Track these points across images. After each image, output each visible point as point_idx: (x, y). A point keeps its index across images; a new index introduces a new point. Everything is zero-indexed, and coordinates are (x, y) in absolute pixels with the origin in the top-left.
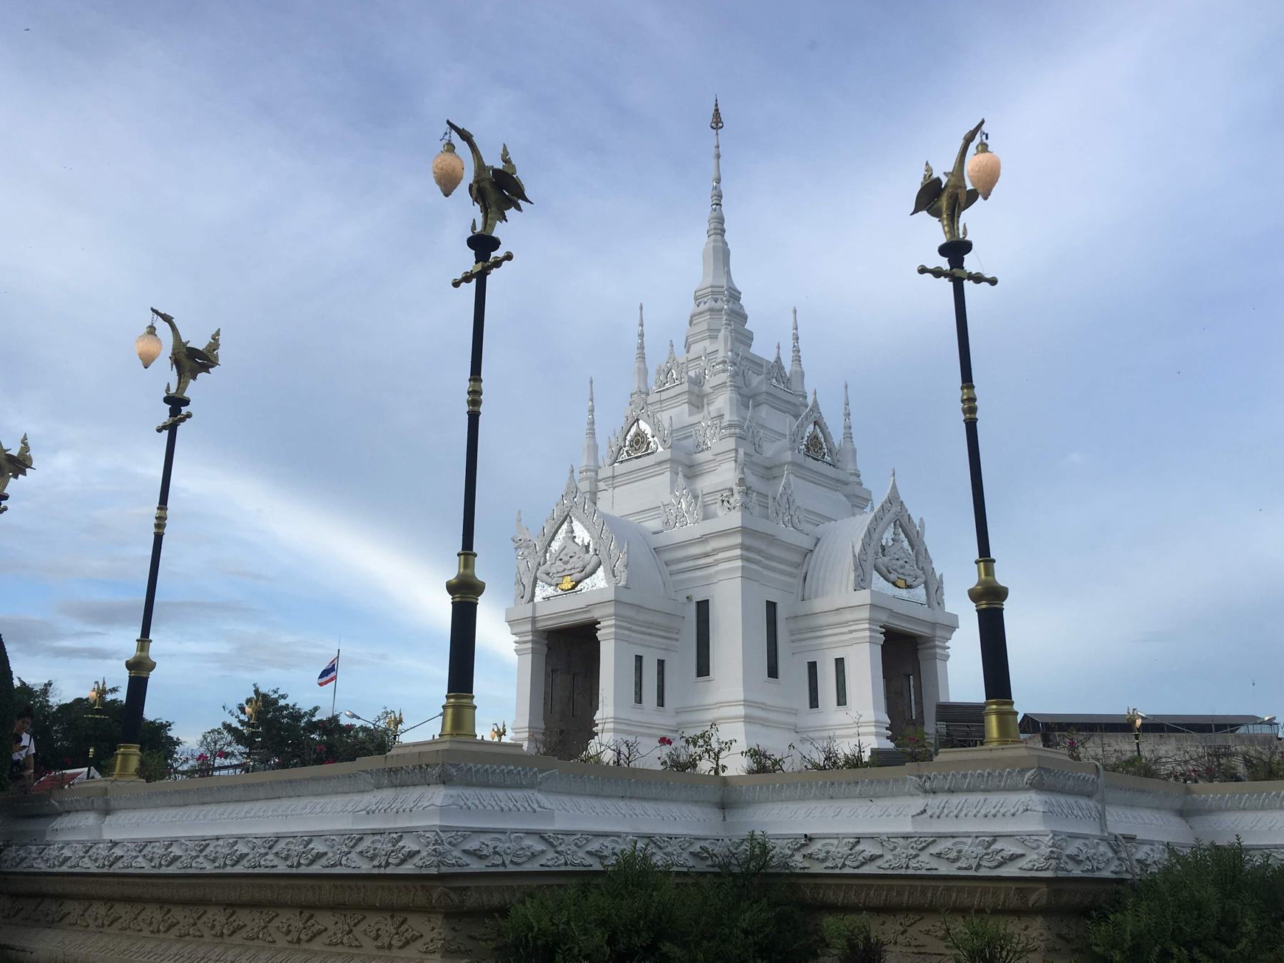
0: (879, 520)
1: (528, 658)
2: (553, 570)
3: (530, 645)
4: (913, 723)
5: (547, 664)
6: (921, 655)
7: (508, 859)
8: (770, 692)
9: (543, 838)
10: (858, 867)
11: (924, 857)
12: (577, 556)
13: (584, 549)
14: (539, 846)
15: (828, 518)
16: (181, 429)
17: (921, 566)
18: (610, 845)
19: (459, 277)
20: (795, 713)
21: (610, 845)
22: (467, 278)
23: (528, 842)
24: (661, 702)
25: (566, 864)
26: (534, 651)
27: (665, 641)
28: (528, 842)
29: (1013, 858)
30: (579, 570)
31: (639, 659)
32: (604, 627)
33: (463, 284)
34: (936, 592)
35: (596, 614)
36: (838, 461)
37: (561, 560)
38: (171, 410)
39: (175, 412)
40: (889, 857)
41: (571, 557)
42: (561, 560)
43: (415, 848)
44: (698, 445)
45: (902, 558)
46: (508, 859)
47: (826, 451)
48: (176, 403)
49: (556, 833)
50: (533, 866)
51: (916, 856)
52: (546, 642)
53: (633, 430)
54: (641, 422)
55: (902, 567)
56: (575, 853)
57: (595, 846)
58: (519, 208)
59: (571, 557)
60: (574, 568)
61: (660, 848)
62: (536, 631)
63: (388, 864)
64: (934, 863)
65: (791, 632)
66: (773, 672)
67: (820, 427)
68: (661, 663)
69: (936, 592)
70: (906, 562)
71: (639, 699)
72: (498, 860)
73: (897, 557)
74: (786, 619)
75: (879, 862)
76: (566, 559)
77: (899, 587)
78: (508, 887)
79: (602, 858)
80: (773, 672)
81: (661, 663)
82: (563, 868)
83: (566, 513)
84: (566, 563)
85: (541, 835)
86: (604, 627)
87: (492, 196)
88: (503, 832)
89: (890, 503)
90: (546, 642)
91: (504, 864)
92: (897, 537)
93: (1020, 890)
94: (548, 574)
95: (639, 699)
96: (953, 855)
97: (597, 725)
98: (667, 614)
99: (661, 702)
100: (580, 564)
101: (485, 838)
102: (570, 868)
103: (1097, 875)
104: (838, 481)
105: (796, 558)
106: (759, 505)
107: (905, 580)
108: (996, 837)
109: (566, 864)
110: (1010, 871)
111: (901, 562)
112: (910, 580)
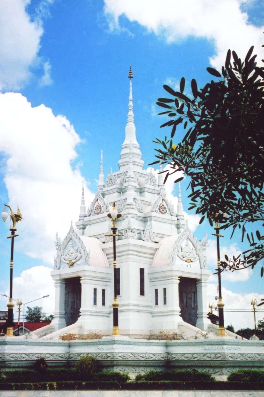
0: (183, 235)
1: (59, 289)
2: (66, 258)
5: (65, 290)
7: (18, 358)
8: (142, 300)
11: (205, 357)
13: (76, 251)
14: (152, 356)
15: (184, 225)
18: (233, 355)
19: (8, 237)
20: (151, 307)
21: (233, 355)
22: (10, 237)
23: (47, 355)
24: (104, 304)
26: (60, 287)
28: (47, 355)
29: (196, 357)
30: (74, 258)
31: (95, 290)
32: (83, 279)
33: (9, 238)
34: (204, 262)
35: (80, 275)
36: (172, 213)
37: (69, 254)
39: (13, 233)
40: (199, 357)
41: (72, 254)
42: (69, 254)
44: (119, 209)
46: (18, 358)
47: (167, 209)
48: (13, 231)
49: (29, 354)
51: (181, 357)
52: (65, 283)
53: (97, 204)
54: (99, 201)
55: (189, 255)
57: (37, 356)
59: (72, 254)
61: (52, 356)
62: (61, 279)
66: (142, 293)
67: (165, 201)
68: (104, 291)
69: (204, 262)
70: (191, 253)
71: (95, 303)
73: (187, 251)
74: (148, 274)
76: (70, 254)
77: (188, 262)
79: (38, 358)
80: (142, 293)
81: (104, 291)
84: (70, 256)
85: (25, 354)
86: (83, 279)
88: (18, 353)
89: (185, 232)
90: (65, 283)
91: (18, 359)
93: (111, 362)
94: (65, 259)
95: (95, 303)
96: (187, 357)
97: (81, 313)
99: (104, 304)
100: (75, 257)
101: (14, 355)
105: (153, 252)
106: (137, 233)
107: (190, 260)
108: (107, 353)
111: (189, 253)
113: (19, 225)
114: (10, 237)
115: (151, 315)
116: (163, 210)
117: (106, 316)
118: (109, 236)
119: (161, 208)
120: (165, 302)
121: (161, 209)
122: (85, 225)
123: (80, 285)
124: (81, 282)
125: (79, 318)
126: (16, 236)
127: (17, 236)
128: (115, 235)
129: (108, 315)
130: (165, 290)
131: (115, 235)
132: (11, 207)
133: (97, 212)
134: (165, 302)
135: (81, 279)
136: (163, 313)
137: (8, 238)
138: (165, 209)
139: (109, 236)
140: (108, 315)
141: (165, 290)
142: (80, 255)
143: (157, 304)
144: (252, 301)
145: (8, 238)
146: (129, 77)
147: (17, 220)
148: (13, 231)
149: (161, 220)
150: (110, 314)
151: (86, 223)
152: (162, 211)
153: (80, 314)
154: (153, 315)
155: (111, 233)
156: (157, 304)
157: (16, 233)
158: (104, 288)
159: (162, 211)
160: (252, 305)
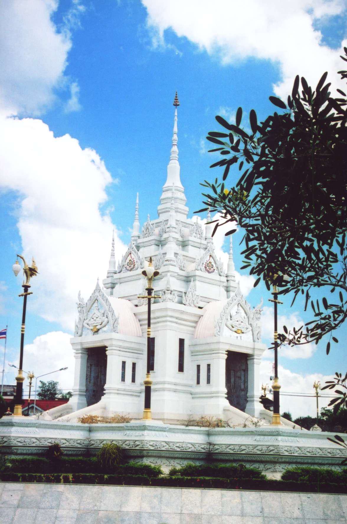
1: (79, 360)
2: (90, 323)
3: (80, 355)
4: (243, 390)
5: (88, 362)
6: (249, 362)
7: (27, 443)
9: (36, 439)
10: (241, 452)
12: (100, 317)
13: (102, 315)
16: (28, 296)
17: (250, 323)
22: (22, 295)
24: (133, 380)
25: (171, 449)
26: (82, 357)
27: (136, 355)
29: (244, 450)
31: (124, 363)
33: (21, 296)
37: (93, 318)
38: (25, 289)
41: (97, 318)
42: (93, 318)
43: (6, 440)
45: (240, 320)
46: (27, 443)
48: (26, 288)
50: (190, 450)
52: (87, 353)
53: (129, 258)
55: (240, 324)
56: (44, 442)
57: (50, 441)
58: (36, 275)
59: (97, 318)
60: (98, 323)
61: (68, 442)
63: (132, 447)
64: (257, 451)
65: (192, 353)
66: (181, 368)
68: (134, 365)
70: (242, 322)
71: (123, 379)
72: (25, 443)
75: (218, 450)
76: (95, 318)
77: (238, 333)
78: (28, 449)
79: (51, 443)
80: (181, 368)
81: (134, 365)
82: (41, 446)
83: (95, 298)
84: (95, 320)
85: (36, 438)
87: (29, 273)
88: (27, 437)
90: (87, 353)
92: (238, 311)
93: (140, 452)
94: (88, 324)
95: (123, 379)
97: (105, 390)
98: (137, 343)
99: (133, 380)
100: (100, 322)
102: (197, 451)
103: (293, 454)
104: (220, 281)
105: (195, 319)
108: (136, 441)
109: (171, 449)
110: (137, 448)
111: (239, 322)
112: (243, 330)
113: (33, 281)
114: (22, 295)
115: (190, 396)
116: (210, 268)
117: (136, 396)
118: (143, 298)
119: (208, 266)
120: (208, 381)
121: (208, 268)
122: (114, 284)
123: (106, 356)
124: (107, 353)
125: (102, 397)
126: (29, 294)
127: (31, 294)
128: (150, 297)
129: (138, 394)
130: (209, 366)
131: (150, 297)
132: (24, 258)
133: (129, 269)
134: (208, 381)
135: (107, 349)
136: (206, 394)
137: (20, 296)
138: (212, 267)
139: (143, 298)
140: (138, 394)
141: (209, 366)
142: (106, 319)
143: (198, 382)
144: (315, 383)
145: (20, 296)
146: (174, 105)
147: (31, 275)
148: (26, 288)
149: (207, 280)
150: (141, 393)
151: (115, 282)
152: (209, 270)
153: (104, 392)
154: (193, 396)
155: (146, 294)
156: (198, 382)
157: (30, 290)
158: (135, 361)
159: (209, 270)
160: (315, 388)
